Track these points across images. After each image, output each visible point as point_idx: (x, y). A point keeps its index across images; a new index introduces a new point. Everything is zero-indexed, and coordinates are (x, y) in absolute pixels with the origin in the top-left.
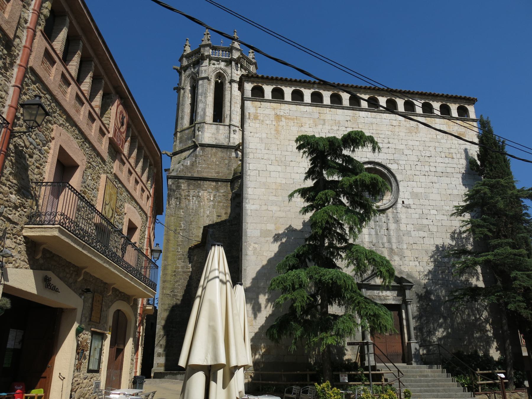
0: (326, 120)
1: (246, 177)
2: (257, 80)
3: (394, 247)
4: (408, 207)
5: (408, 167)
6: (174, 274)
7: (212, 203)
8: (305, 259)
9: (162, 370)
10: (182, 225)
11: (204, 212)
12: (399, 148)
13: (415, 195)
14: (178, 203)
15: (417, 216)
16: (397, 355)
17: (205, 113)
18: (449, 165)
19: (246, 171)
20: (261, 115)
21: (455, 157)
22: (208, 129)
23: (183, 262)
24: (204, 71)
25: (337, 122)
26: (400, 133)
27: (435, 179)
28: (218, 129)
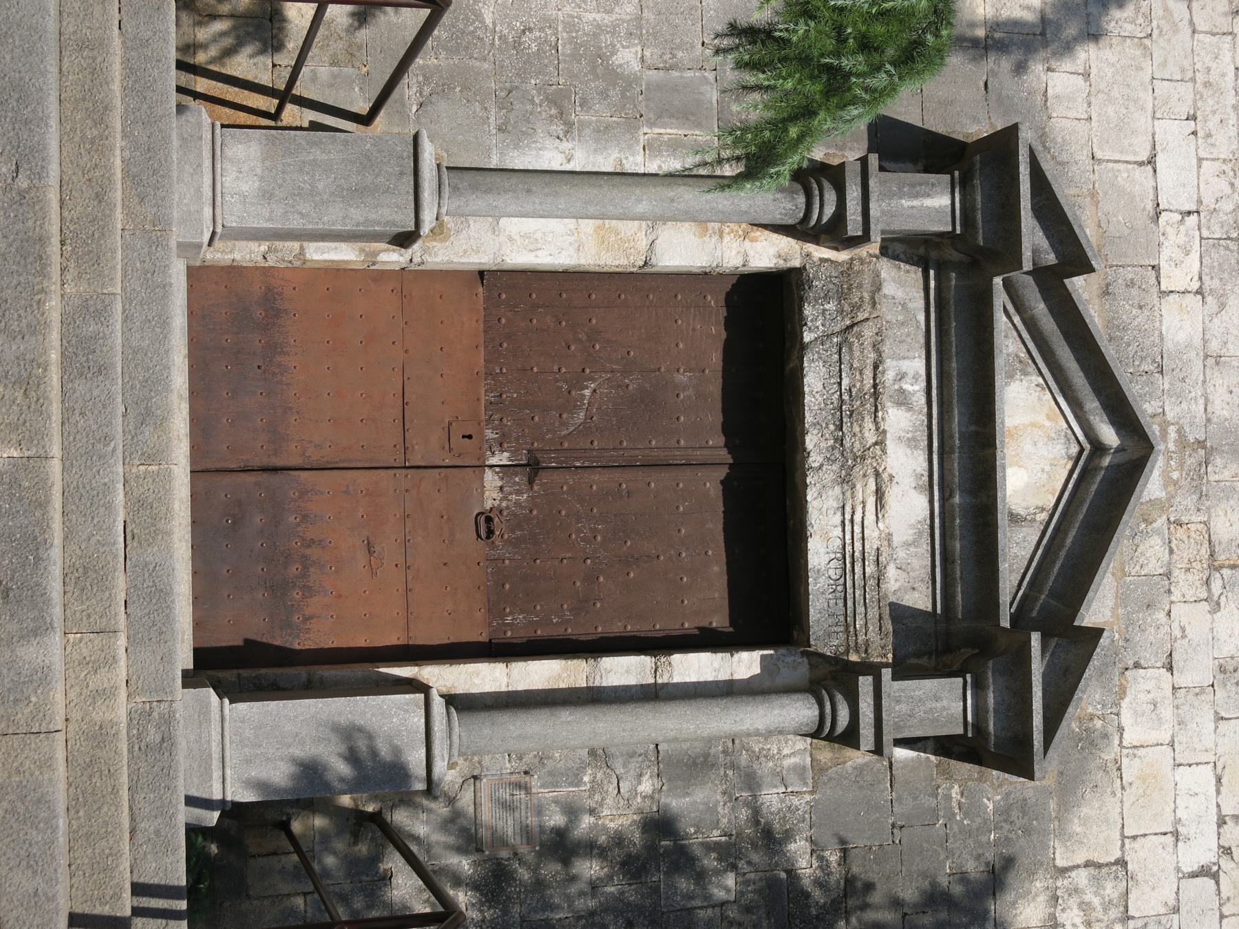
9: (884, 671)
16: (278, 588)
24: (111, 378)
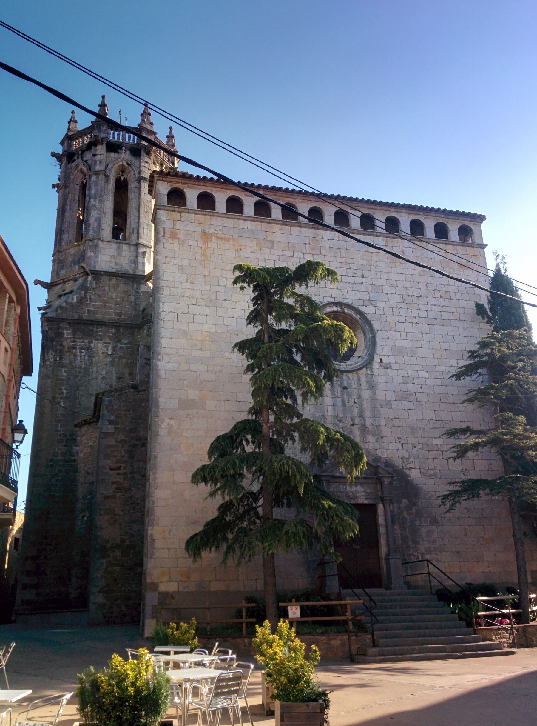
0: (275, 243)
1: (158, 323)
2: (175, 179)
3: (368, 423)
4: (388, 367)
5: (388, 311)
6: (50, 464)
7: (109, 359)
8: (241, 440)
10: (64, 391)
11: (97, 372)
12: (377, 284)
13: (398, 351)
14: (58, 359)
15: (400, 380)
17: (99, 226)
18: (445, 309)
19: (159, 314)
20: (182, 232)
21: (453, 297)
22: (104, 248)
23: (65, 446)
24: (98, 162)
25: (290, 245)
26: (378, 263)
27: (426, 328)
28: (119, 250)
